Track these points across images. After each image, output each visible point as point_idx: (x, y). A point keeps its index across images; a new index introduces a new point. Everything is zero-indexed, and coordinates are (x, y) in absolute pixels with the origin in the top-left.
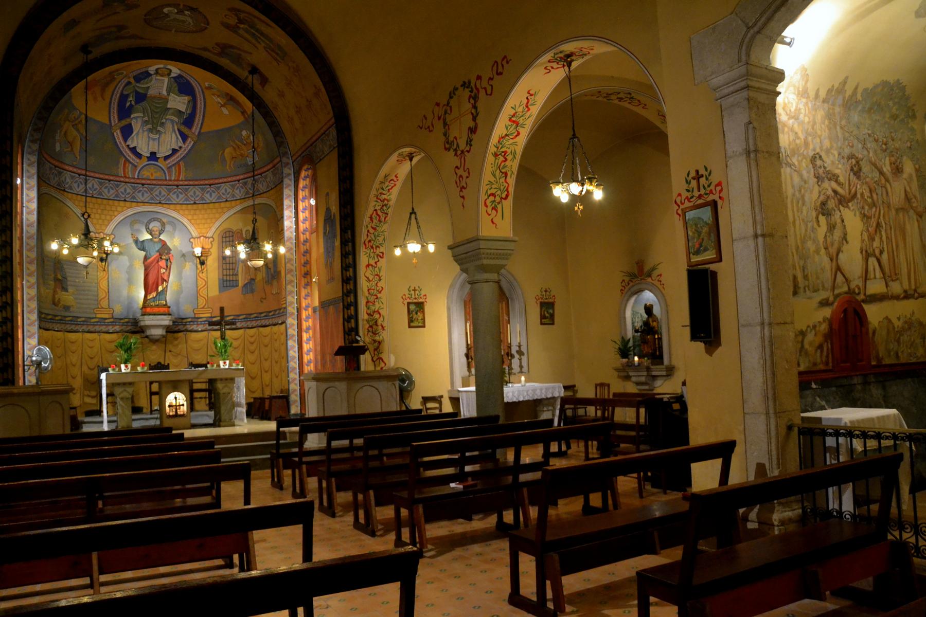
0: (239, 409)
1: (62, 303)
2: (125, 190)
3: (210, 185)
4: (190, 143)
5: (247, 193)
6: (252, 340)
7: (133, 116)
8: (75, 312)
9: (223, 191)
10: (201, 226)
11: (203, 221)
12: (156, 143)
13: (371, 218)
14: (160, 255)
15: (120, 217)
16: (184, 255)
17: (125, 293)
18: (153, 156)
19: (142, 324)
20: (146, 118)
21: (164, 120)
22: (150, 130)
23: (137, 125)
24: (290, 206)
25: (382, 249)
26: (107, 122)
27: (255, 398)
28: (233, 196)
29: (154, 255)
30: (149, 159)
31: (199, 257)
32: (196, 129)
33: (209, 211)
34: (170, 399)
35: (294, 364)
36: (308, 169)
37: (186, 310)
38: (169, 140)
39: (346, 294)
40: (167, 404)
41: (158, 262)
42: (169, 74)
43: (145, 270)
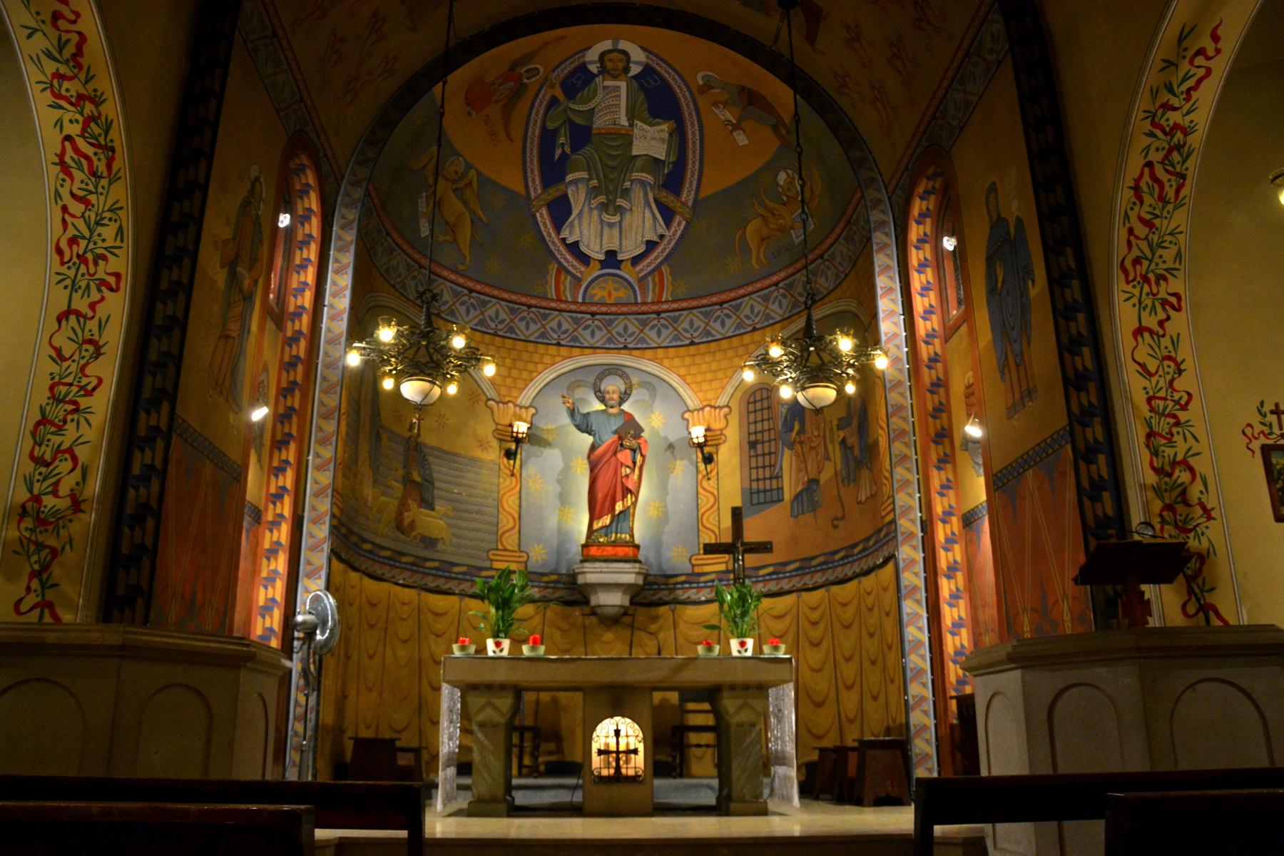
0: (779, 770)
1: (419, 530)
2: (560, 325)
3: (721, 304)
4: (679, 225)
5: (795, 305)
6: (814, 616)
7: (569, 178)
8: (447, 552)
9: (747, 311)
10: (705, 386)
11: (709, 376)
12: (616, 231)
13: (1137, 189)
14: (620, 438)
15: (548, 375)
16: (671, 447)
17: (552, 522)
18: (611, 259)
19: (581, 580)
20: (594, 182)
21: (627, 184)
22: (604, 207)
23: (578, 198)
24: (891, 290)
25: (1175, 285)
26: (523, 192)
27: (823, 751)
28: (768, 317)
29: (609, 439)
30: (604, 264)
31: (700, 446)
32: (688, 195)
33: (719, 356)
34: (603, 734)
35: (919, 660)
36: (935, 175)
37: (677, 557)
38: (640, 225)
39: (1079, 419)
40: (595, 746)
41: (615, 453)
42: (626, 70)
43: (592, 471)
